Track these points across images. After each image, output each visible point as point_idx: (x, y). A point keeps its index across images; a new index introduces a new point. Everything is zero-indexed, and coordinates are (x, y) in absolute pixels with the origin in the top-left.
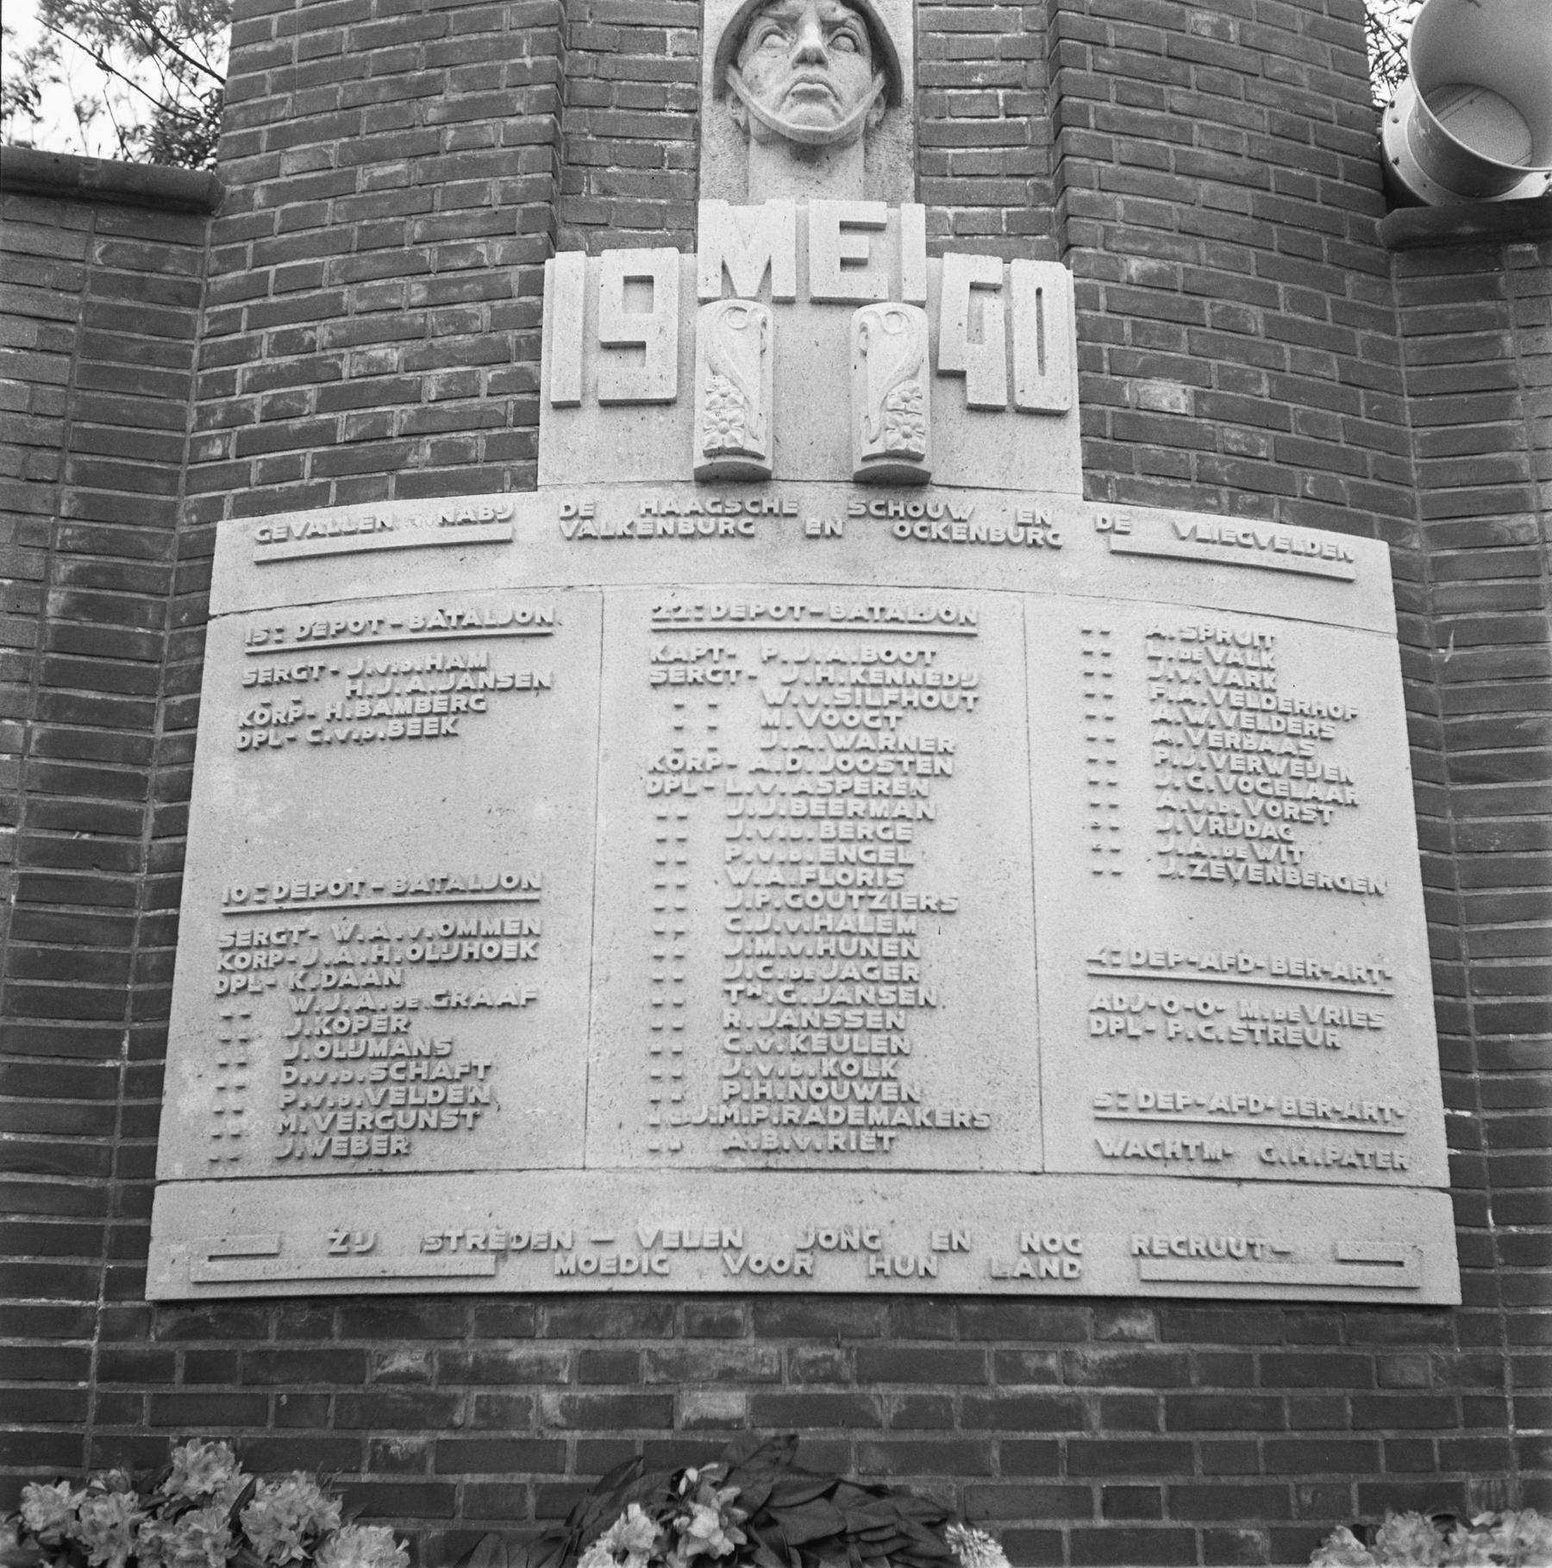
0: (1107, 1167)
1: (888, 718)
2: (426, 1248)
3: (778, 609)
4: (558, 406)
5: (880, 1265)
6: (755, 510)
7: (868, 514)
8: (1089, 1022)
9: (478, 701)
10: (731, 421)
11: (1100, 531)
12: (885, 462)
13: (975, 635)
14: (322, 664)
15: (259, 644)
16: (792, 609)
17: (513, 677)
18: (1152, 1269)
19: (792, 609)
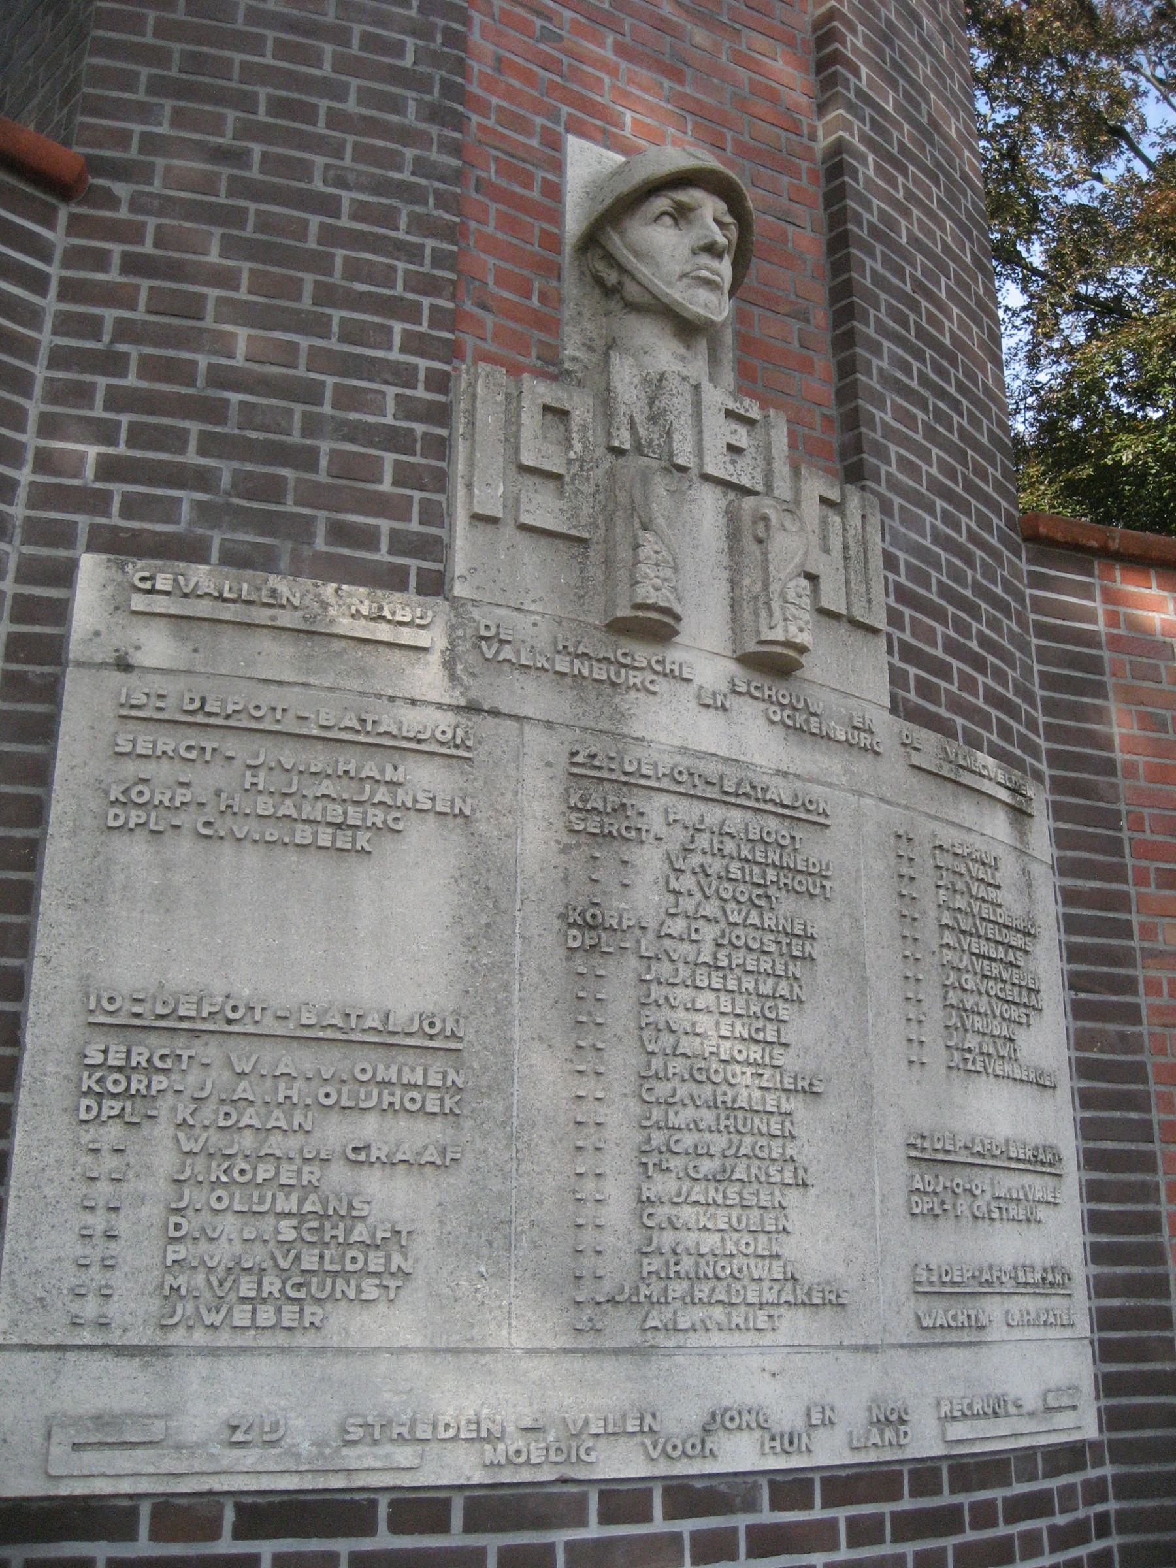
0: (927, 1338)
1: (203, 749)
2: (86, 1204)
3: (258, 707)
4: (477, 518)
5: (289, 1093)
6: (658, 668)
7: (748, 693)
8: (107, 814)
9: (396, 819)
10: (665, 580)
11: (904, 745)
12: (778, 649)
13: (827, 826)
14: (216, 745)
15: (133, 707)
16: (274, 709)
17: (433, 799)
18: (958, 1431)
19: (274, 709)
